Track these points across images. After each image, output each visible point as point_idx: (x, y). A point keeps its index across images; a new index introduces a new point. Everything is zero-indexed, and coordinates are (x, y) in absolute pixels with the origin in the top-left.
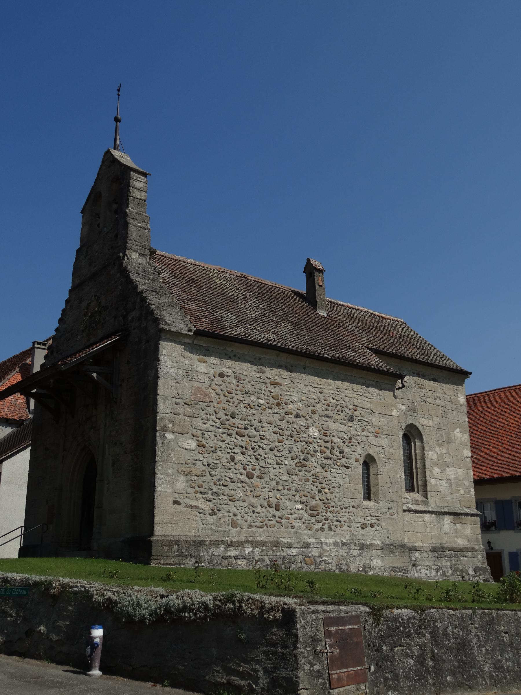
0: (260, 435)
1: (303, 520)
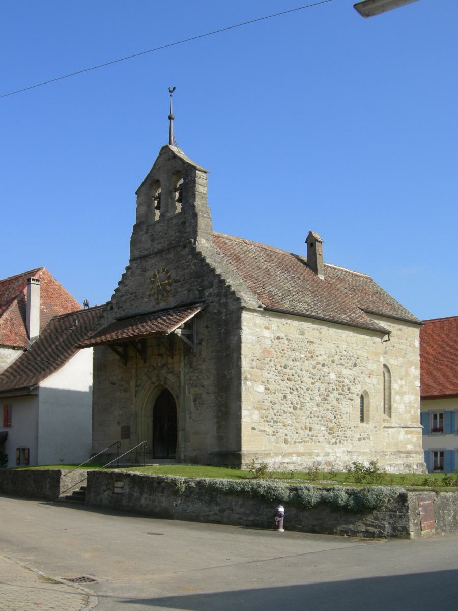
1: (325, 437)
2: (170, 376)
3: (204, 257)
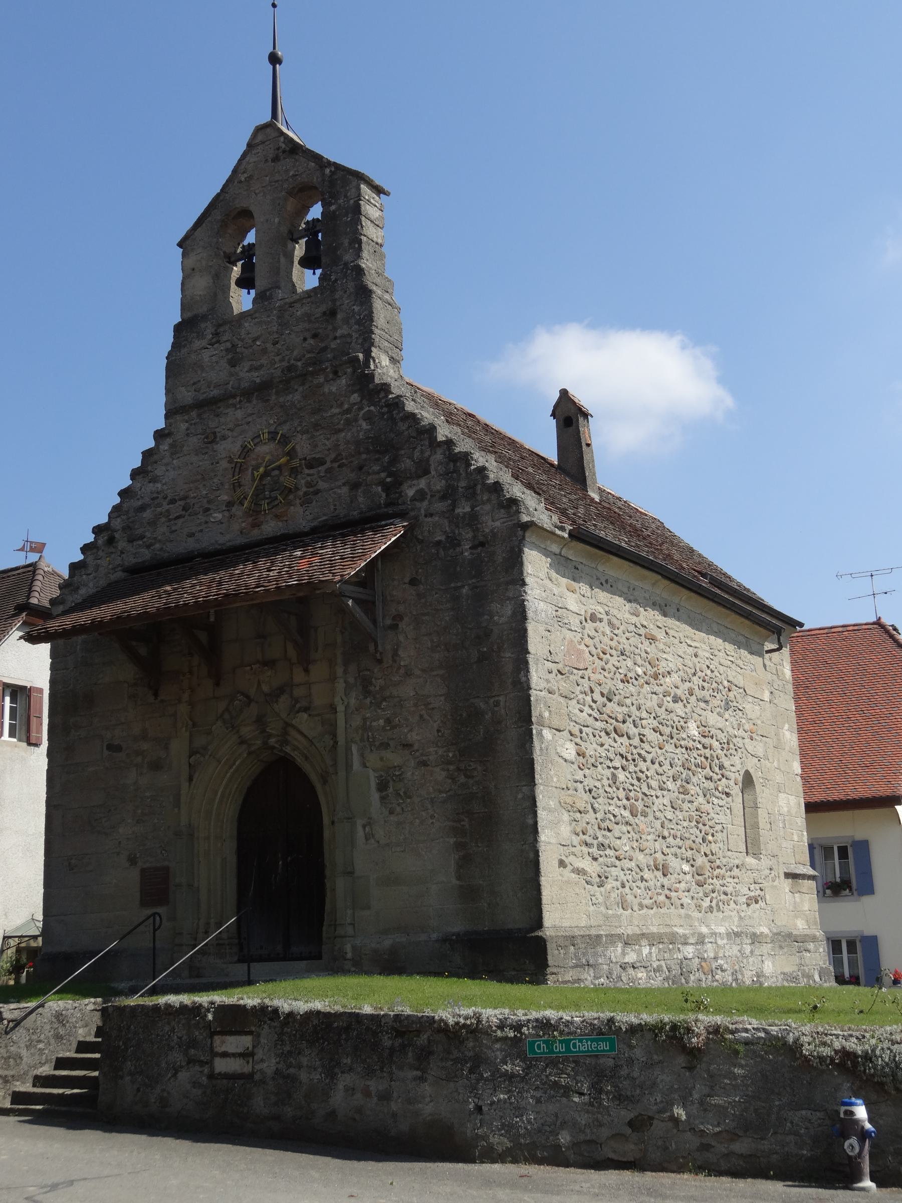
0: (640, 734)
2: (302, 720)
3: (399, 397)
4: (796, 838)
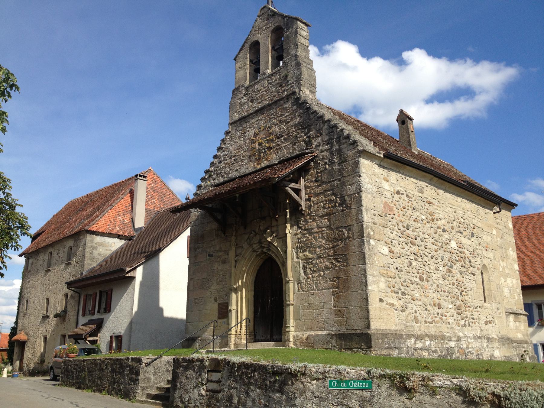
4: (516, 298)
